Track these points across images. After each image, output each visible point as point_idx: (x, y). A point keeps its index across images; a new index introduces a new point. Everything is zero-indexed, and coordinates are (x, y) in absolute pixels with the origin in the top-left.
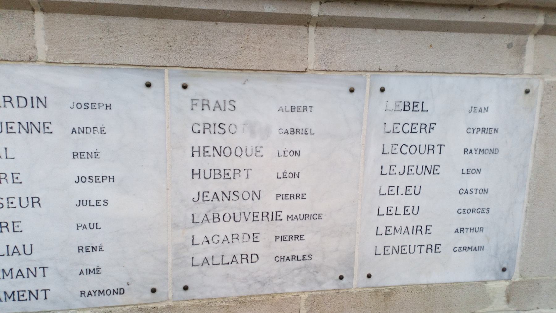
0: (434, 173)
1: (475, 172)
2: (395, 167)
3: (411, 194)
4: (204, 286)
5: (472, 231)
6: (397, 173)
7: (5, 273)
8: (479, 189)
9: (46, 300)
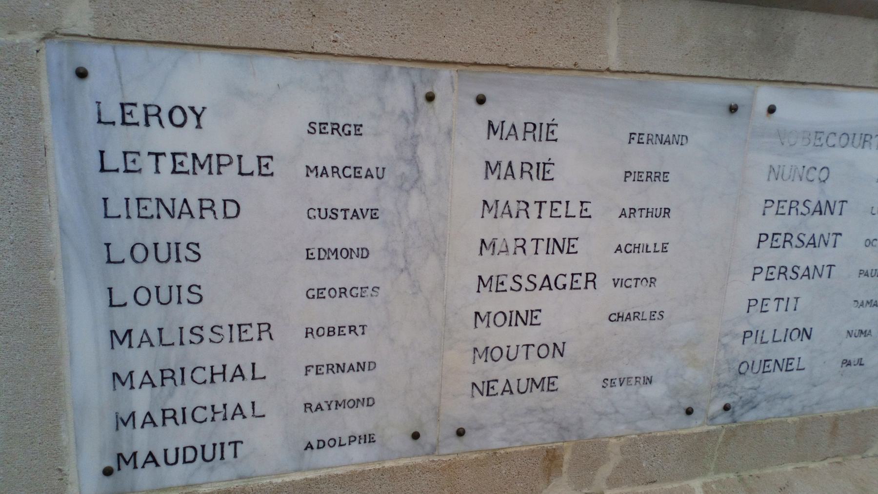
0: (498, 289)
1: (625, 282)
2: (528, 289)
3: (506, 291)
4: (693, 319)
5: (650, 215)
6: (508, 290)
7: (117, 337)
8: (641, 279)
9: (166, 448)
